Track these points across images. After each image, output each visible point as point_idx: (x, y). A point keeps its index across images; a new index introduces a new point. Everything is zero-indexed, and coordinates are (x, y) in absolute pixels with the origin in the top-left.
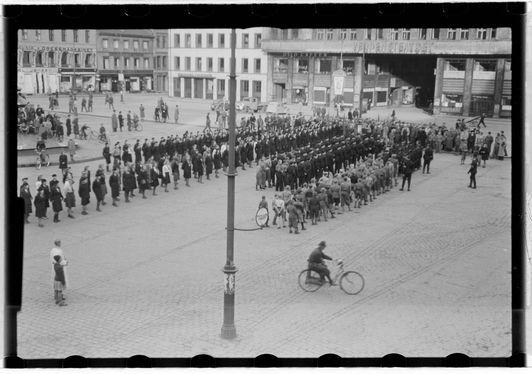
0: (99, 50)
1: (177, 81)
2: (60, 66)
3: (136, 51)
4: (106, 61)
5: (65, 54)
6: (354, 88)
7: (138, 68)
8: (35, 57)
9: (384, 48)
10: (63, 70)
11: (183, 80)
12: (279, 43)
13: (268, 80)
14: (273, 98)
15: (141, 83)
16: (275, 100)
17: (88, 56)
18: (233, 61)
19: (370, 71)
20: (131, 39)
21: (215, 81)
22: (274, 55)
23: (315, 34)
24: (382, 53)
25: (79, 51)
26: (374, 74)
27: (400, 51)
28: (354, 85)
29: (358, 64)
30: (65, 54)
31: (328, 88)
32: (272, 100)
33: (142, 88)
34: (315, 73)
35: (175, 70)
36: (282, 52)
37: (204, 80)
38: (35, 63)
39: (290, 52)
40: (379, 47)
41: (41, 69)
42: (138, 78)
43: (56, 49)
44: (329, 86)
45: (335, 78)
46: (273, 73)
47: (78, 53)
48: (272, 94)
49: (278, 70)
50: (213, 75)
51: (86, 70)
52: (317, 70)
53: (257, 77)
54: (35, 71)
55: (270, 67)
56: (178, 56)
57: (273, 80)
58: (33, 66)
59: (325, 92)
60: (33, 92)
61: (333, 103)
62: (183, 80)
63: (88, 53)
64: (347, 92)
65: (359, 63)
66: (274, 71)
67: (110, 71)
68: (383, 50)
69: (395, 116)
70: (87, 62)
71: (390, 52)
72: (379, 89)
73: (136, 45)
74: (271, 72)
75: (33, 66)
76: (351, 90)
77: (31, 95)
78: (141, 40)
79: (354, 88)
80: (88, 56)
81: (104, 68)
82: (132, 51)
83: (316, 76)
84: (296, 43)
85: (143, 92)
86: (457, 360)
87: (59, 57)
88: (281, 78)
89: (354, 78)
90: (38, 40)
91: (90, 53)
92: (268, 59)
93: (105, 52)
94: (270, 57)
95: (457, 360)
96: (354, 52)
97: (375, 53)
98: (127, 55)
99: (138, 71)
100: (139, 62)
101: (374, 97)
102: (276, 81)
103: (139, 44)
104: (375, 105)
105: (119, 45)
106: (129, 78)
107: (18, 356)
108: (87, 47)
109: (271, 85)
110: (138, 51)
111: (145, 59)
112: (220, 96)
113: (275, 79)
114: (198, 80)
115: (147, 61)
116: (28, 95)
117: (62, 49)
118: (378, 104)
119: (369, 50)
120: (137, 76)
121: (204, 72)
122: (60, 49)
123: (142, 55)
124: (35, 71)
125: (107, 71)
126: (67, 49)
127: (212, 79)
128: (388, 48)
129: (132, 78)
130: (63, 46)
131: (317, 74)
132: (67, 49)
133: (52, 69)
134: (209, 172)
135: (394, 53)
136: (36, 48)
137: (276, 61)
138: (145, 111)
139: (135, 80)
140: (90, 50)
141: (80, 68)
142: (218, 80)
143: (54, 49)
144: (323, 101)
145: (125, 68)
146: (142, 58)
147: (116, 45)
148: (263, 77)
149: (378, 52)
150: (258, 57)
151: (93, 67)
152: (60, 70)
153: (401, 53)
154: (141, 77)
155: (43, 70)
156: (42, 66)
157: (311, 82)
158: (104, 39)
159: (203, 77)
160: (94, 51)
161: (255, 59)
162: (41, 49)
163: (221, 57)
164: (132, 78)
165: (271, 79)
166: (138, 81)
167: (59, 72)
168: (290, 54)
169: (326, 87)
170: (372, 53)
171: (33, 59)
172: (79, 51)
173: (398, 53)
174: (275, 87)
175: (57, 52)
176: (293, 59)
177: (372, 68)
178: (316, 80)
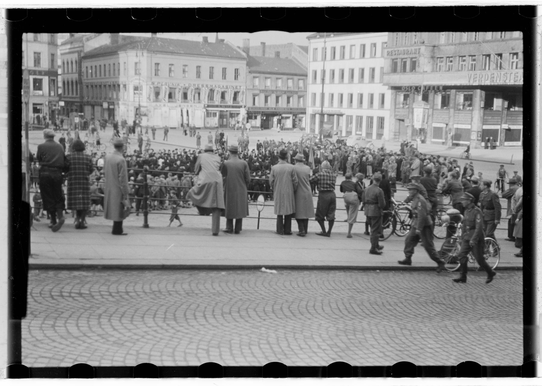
0: (248, 88)
1: (313, 116)
2: (206, 103)
3: (289, 89)
4: (257, 98)
5: (212, 91)
6: (471, 124)
7: (291, 105)
8: (180, 93)
9: (498, 79)
10: (208, 106)
11: (317, 116)
12: (398, 76)
13: (391, 116)
14: (395, 135)
15: (294, 121)
16: (397, 137)
17: (236, 94)
18: (323, 95)
19: (497, 106)
20: (285, 77)
21: (344, 117)
22: (397, 89)
23: (435, 66)
24: (496, 84)
25: (227, 88)
26: (500, 109)
27: (515, 81)
28: (472, 121)
29: (476, 97)
30: (212, 91)
31: (447, 125)
32: (393, 137)
33: (294, 126)
34: (435, 108)
35: (311, 107)
36: (400, 85)
37: (335, 116)
38: (180, 99)
39: (407, 85)
40: (494, 77)
41: (186, 104)
42: (291, 116)
43: (203, 86)
44: (447, 122)
45: (415, 110)
46: (395, 108)
47: (226, 90)
48: (393, 131)
49: (401, 106)
50: (342, 111)
51: (233, 107)
52: (437, 105)
53: (381, 113)
54: (180, 106)
55: (393, 103)
56: (314, 92)
57: (395, 116)
58: (178, 102)
59: (444, 129)
60: (177, 126)
61: (451, 141)
62: (317, 116)
63: (236, 90)
64: (485, 130)
65: (479, 97)
66: (397, 107)
67: (260, 108)
68: (498, 81)
69: (470, 152)
70: (235, 99)
71: (504, 84)
72: (505, 126)
73: (290, 82)
74: (393, 107)
75: (178, 102)
76: (469, 127)
77: (175, 128)
78: (296, 78)
79: (471, 124)
80: (236, 94)
81: (254, 104)
82: (285, 89)
83: (434, 111)
84: (414, 75)
85: (295, 130)
86: (82, 371)
87: (205, 94)
88: (402, 113)
89: (472, 114)
90: (185, 77)
91: (238, 90)
92: (392, 94)
93: (255, 90)
94: (393, 91)
95: (82, 371)
96: (468, 84)
97: (489, 84)
98: (279, 93)
99: (291, 109)
100: (293, 99)
101: (501, 136)
102: (398, 117)
103: (293, 83)
104: (501, 145)
105: (271, 82)
106: (280, 115)
107: (23, 364)
108: (235, 84)
109: (393, 121)
110: (292, 89)
111: (299, 97)
112: (313, 130)
113: (397, 115)
114: (331, 115)
115: (302, 99)
116: (171, 128)
117: (209, 86)
118: (506, 143)
119: (483, 82)
120: (291, 113)
121: (335, 109)
122: (207, 86)
123: (296, 93)
124: (180, 106)
125: (256, 108)
126: (214, 86)
127: (342, 115)
128: (502, 78)
129: (284, 115)
130: (210, 83)
131: (437, 109)
132: (214, 86)
133: (198, 105)
134: (161, 189)
135: (509, 84)
136: (182, 85)
137: (399, 95)
138: (201, 139)
139: (288, 118)
140: (238, 87)
141: (228, 104)
142: (347, 116)
143: (200, 86)
144: (441, 138)
145: (276, 105)
146: (296, 97)
147: (268, 82)
148: (387, 113)
149: (492, 84)
150: (383, 92)
151: (241, 104)
152: (206, 106)
153: (516, 83)
154: (295, 115)
155: (188, 106)
156: (160, 101)
157: (452, 119)
158: (254, 77)
159: (333, 113)
160: (243, 88)
161: (369, 94)
162: (187, 85)
163: (351, 92)
164: (284, 115)
165: (393, 115)
166: (291, 118)
167: (205, 107)
168: (408, 87)
169: (444, 123)
170: (486, 84)
171: (179, 96)
172: (227, 88)
173: (513, 84)
174: (398, 124)
175: (204, 88)
176: (414, 93)
177: (498, 103)
178: (435, 116)
